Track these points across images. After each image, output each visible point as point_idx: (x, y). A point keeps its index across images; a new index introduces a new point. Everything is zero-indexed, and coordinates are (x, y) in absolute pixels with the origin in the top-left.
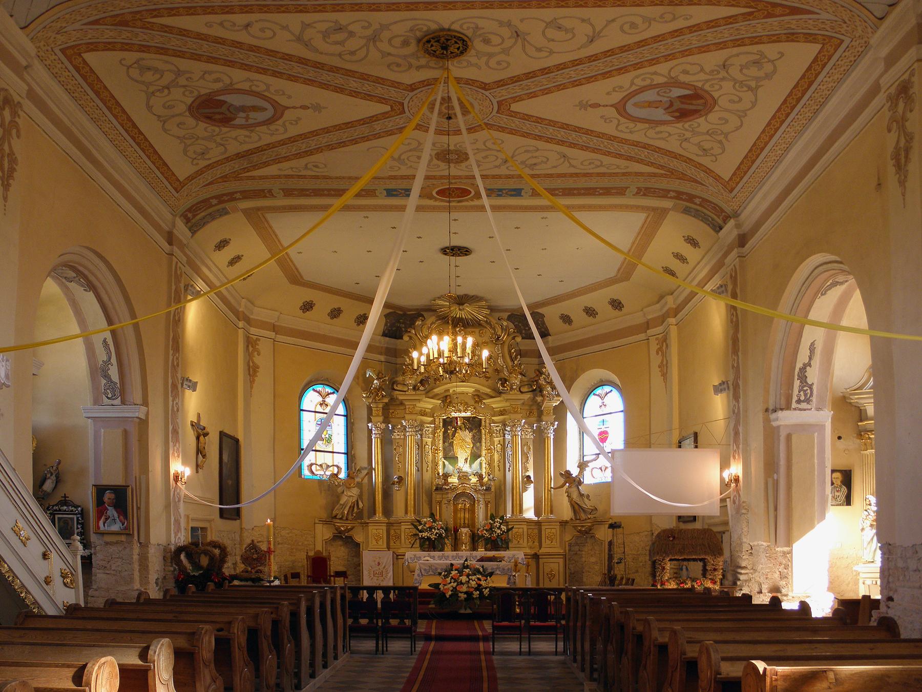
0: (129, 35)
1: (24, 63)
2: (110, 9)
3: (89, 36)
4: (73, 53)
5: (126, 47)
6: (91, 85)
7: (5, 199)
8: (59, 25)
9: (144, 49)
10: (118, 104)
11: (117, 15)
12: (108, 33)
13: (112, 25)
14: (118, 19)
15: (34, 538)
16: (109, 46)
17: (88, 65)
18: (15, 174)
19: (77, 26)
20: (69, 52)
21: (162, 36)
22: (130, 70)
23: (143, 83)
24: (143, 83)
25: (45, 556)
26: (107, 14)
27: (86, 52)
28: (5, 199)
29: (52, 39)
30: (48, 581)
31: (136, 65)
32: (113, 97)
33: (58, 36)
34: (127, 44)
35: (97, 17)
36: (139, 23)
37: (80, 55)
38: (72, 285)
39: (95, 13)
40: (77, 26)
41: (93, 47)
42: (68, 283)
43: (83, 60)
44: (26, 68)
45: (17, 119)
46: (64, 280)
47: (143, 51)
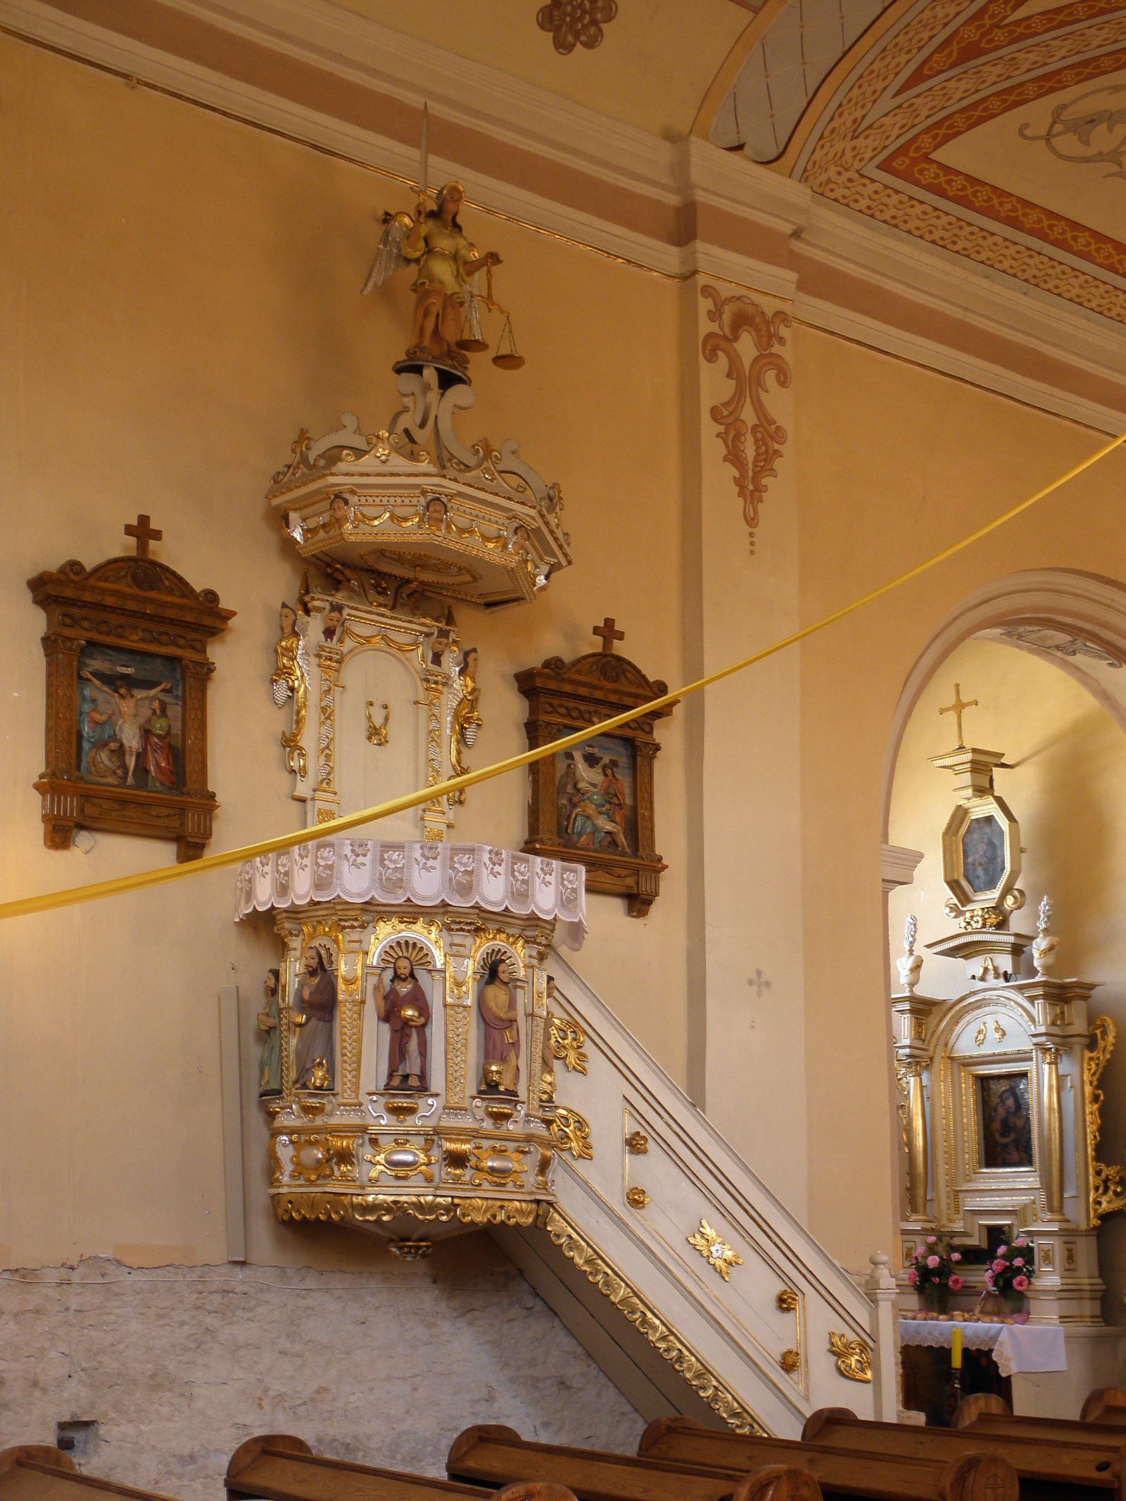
0: (998, 69)
1: (788, 229)
2: (926, 35)
3: (925, 112)
4: (909, 162)
5: (1013, 98)
6: (988, 212)
7: (751, 521)
8: (848, 118)
9: (1049, 83)
10: (1074, 225)
11: (948, 41)
12: (958, 88)
13: (952, 67)
14: (955, 47)
15: (753, 1262)
16: (978, 114)
17: (958, 173)
18: (778, 464)
19: (886, 102)
20: (899, 164)
21: (1064, 38)
22: (1054, 141)
23: (1100, 158)
24: (1100, 158)
25: (784, 1303)
26: (927, 52)
27: (936, 147)
28: (751, 521)
29: (849, 154)
30: (789, 1363)
31: (1058, 128)
32: (1051, 215)
33: (860, 142)
34: (1009, 91)
35: (913, 66)
36: (999, 35)
37: (926, 159)
38: (1080, 659)
39: (903, 58)
40: (886, 102)
41: (946, 130)
42: (1071, 659)
43: (942, 166)
44: (796, 234)
45: (777, 348)
46: (1059, 654)
47: (1052, 90)
